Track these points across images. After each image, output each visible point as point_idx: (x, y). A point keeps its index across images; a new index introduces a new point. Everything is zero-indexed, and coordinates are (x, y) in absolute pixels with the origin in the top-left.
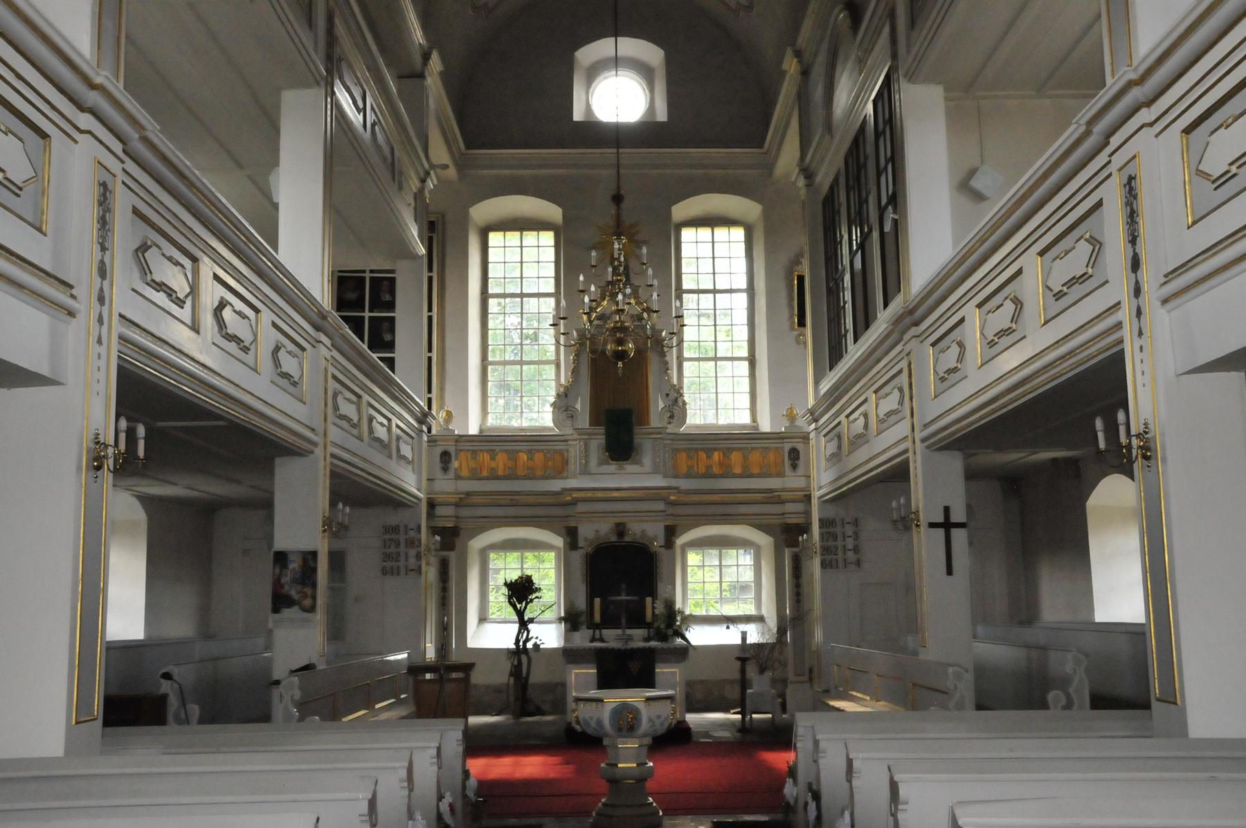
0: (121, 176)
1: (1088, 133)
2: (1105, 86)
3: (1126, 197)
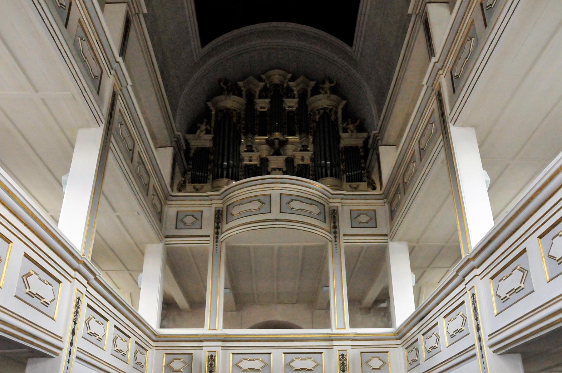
0: (85, 292)
1: (456, 275)
2: (462, 259)
3: (472, 301)
